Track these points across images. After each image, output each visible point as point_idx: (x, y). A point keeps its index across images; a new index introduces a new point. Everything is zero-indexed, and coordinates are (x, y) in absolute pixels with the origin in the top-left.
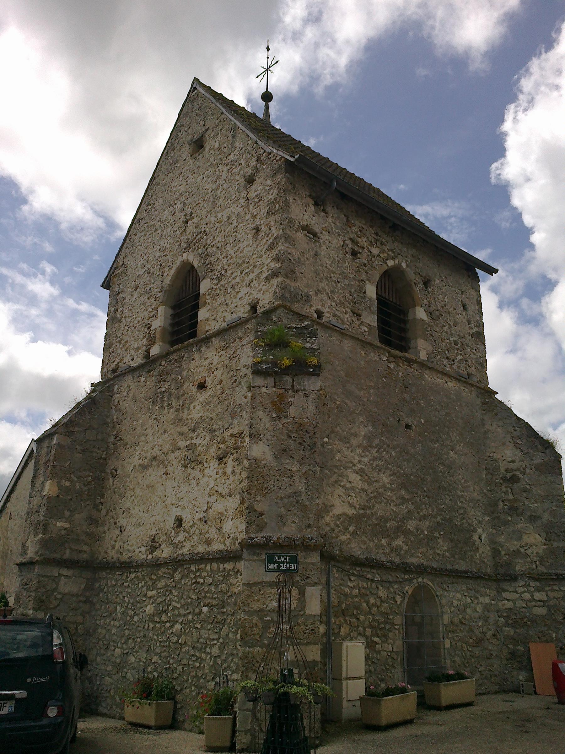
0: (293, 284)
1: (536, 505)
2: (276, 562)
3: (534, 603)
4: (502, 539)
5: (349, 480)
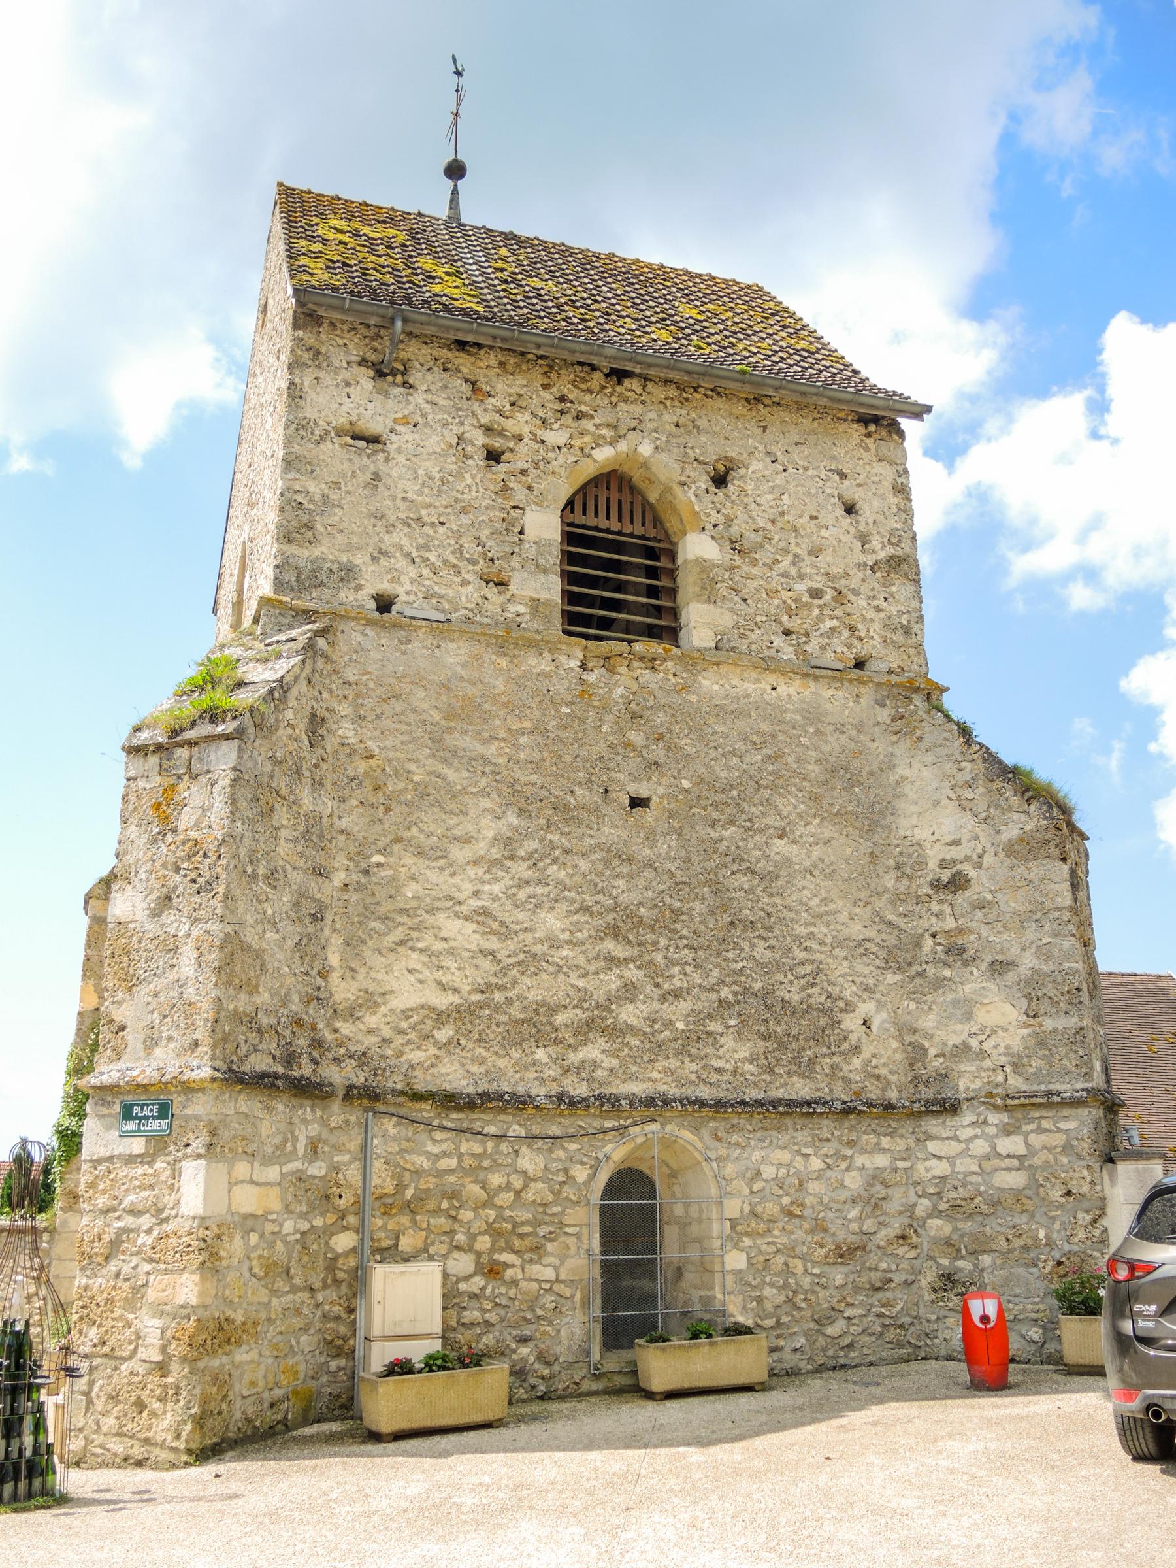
0: (306, 553)
1: (1005, 937)
2: (137, 1118)
3: (996, 1162)
4: (928, 1022)
5: (443, 934)
